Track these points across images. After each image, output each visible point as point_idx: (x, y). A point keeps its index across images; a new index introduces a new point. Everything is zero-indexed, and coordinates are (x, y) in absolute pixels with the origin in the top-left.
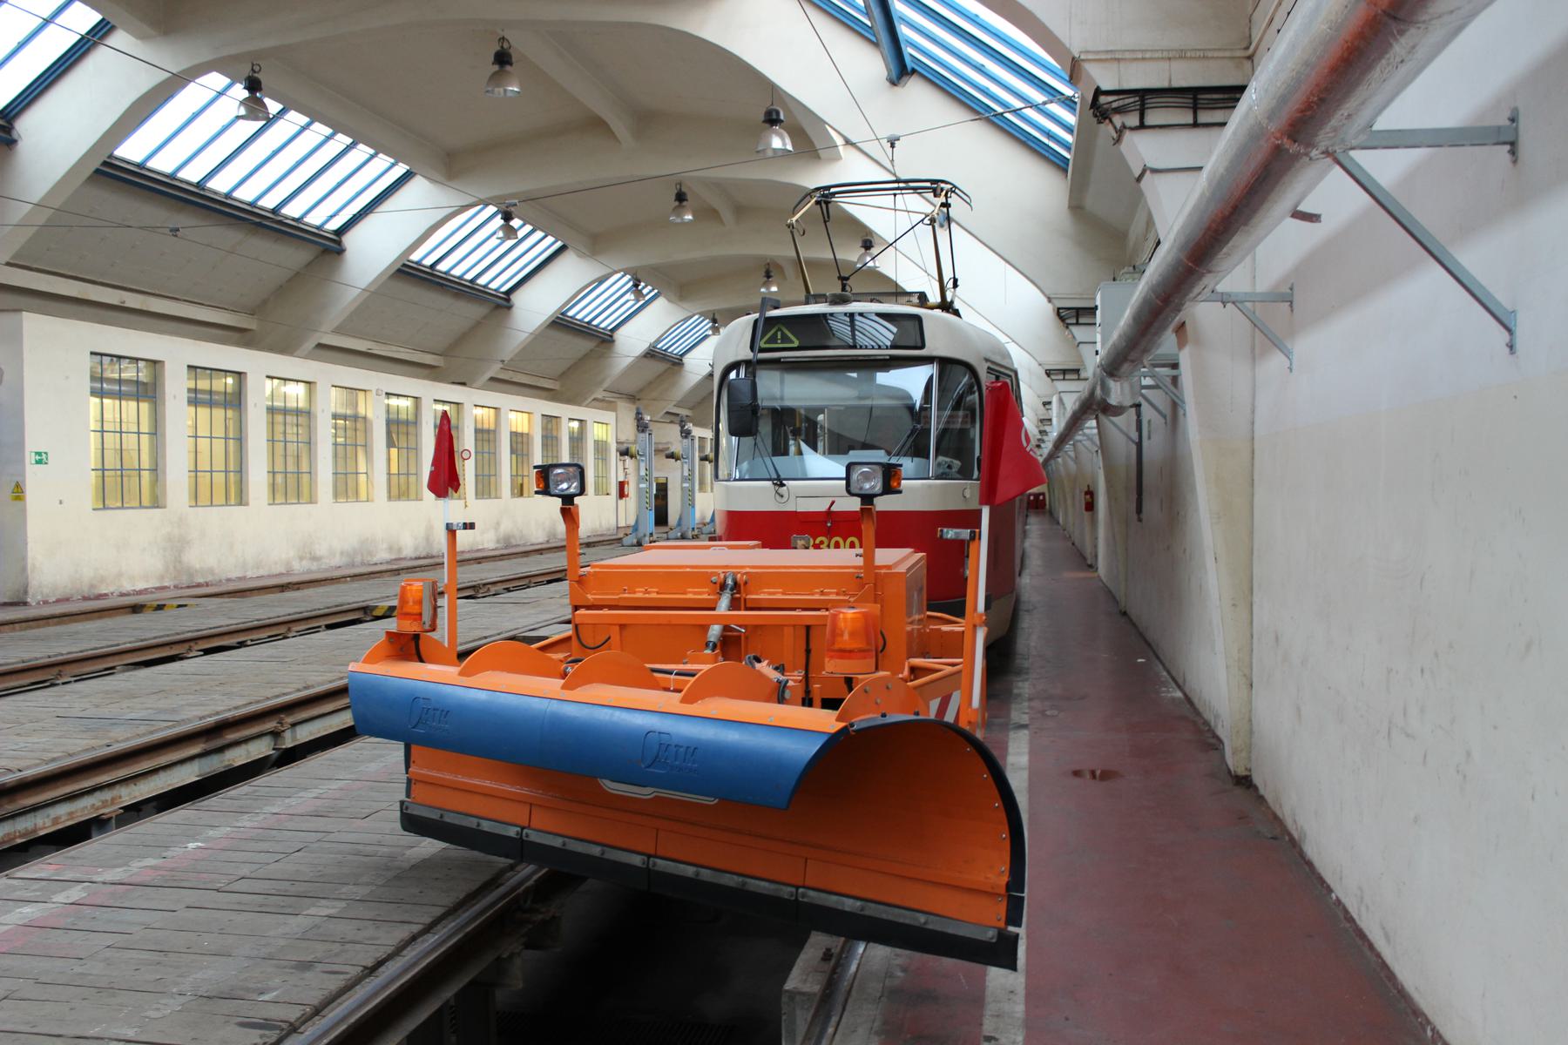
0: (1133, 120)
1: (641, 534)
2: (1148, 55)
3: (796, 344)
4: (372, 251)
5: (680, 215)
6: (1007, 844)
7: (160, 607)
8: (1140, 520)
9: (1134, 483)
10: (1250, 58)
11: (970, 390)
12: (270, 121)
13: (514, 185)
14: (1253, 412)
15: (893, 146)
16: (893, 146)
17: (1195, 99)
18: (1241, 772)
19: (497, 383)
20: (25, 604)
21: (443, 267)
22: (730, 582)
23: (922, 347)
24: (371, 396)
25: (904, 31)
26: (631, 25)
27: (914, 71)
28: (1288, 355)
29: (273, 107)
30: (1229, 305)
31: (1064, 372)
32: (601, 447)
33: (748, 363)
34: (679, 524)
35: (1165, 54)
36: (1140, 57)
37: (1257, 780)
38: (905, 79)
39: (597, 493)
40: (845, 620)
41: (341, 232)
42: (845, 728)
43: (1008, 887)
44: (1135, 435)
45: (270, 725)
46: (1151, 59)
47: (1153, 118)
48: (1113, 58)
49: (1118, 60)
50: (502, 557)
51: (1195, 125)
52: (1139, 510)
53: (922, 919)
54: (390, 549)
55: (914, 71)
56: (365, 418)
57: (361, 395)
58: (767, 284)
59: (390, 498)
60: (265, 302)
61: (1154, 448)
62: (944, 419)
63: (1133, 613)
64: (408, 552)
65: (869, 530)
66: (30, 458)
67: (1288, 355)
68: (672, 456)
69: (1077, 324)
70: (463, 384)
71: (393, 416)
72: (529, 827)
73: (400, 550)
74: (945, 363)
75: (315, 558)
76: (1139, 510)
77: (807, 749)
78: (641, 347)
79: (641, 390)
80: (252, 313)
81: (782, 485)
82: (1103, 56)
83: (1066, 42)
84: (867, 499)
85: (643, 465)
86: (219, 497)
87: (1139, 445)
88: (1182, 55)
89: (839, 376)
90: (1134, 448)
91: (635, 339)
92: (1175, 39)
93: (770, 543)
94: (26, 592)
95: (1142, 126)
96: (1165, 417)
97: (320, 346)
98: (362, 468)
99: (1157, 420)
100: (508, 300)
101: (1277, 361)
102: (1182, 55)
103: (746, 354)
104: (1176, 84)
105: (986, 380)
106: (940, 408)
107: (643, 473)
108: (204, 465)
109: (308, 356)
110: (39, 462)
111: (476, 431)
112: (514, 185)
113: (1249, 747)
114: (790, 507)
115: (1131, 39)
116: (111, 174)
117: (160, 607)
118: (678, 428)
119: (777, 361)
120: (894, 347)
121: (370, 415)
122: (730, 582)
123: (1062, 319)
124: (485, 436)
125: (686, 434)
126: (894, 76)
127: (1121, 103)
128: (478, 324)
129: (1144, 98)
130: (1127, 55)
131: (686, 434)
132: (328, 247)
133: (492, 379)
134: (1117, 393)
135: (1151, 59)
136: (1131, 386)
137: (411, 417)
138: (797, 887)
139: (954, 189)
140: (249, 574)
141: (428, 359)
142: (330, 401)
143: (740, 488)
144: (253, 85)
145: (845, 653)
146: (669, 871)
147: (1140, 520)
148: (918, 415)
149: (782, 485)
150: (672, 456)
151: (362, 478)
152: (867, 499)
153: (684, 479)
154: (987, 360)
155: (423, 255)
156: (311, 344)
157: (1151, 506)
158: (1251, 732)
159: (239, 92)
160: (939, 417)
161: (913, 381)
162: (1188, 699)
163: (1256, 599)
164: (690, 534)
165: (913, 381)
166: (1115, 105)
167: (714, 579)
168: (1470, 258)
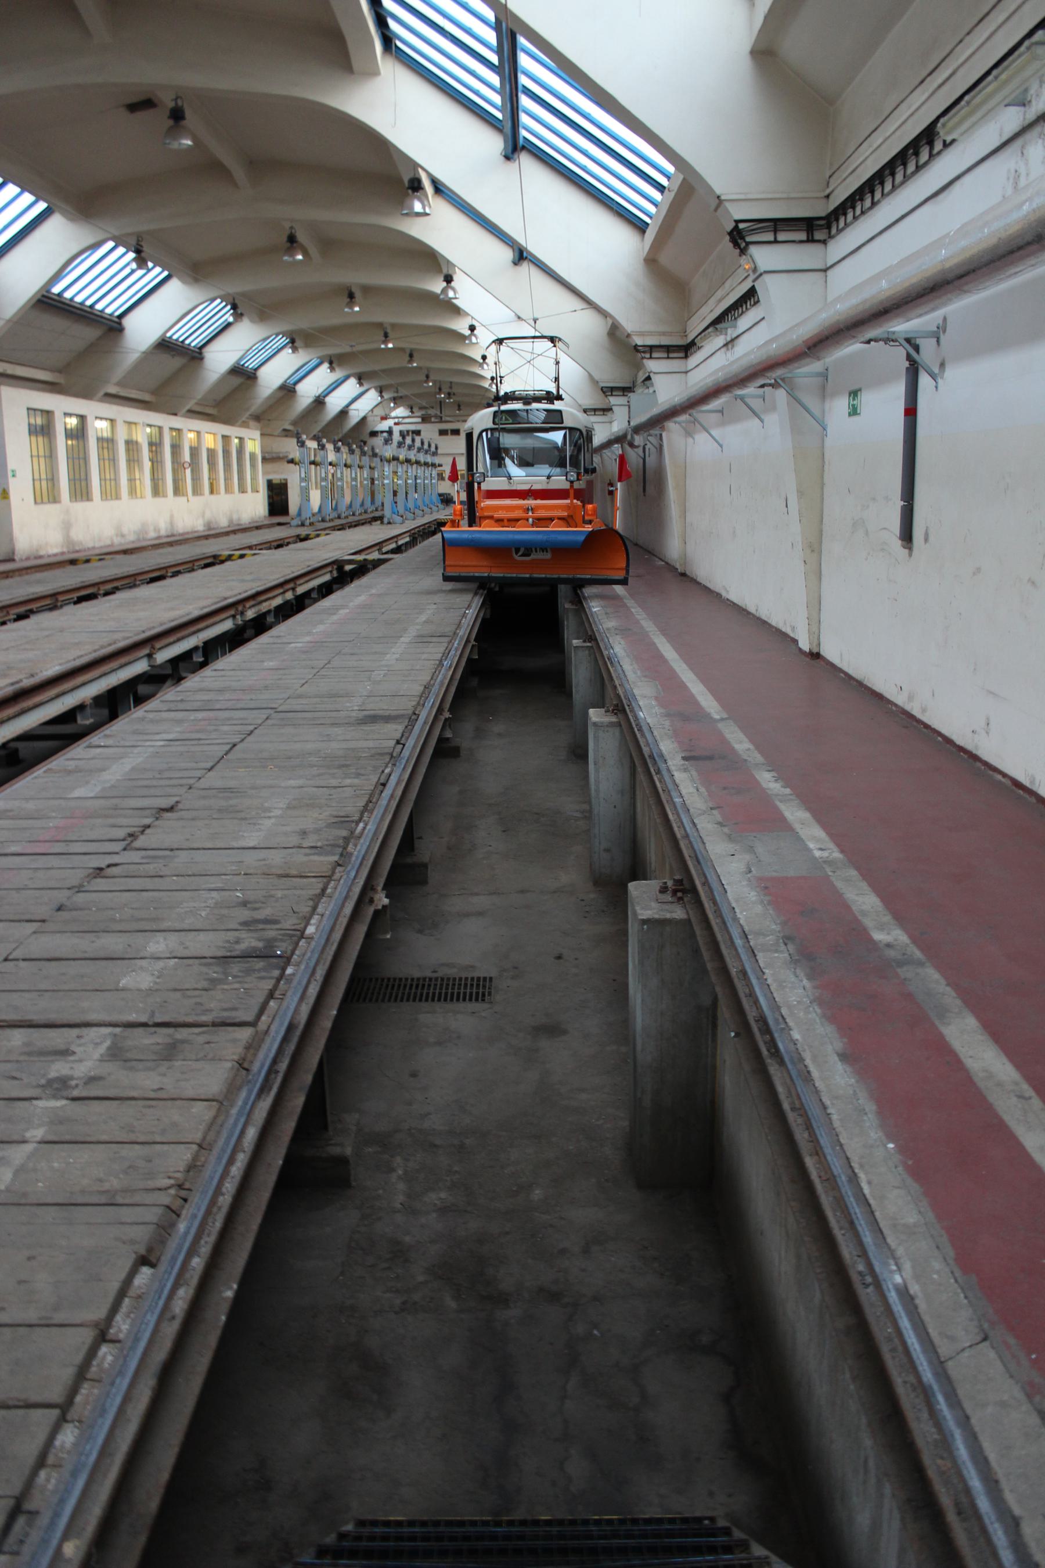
0: (648, 356)
1: (303, 517)
4: (144, 329)
7: (88, 561)
12: (149, 270)
13: (237, 287)
19: (193, 413)
20: (13, 560)
21: (187, 342)
24: (139, 428)
25: (392, 24)
29: (150, 265)
31: (595, 410)
32: (253, 456)
33: (492, 430)
34: (299, 514)
36: (650, 333)
39: (105, 496)
41: (121, 316)
45: (291, 585)
47: (654, 355)
48: (642, 334)
50: (206, 537)
51: (668, 358)
54: (155, 530)
56: (137, 442)
57: (133, 426)
58: (385, 342)
59: (36, 502)
60: (68, 365)
61: (651, 461)
63: (640, 542)
64: (163, 533)
66: (10, 474)
68: (292, 461)
70: (175, 414)
71: (100, 435)
73: (159, 531)
74: (571, 429)
75: (123, 536)
77: (582, 538)
78: (277, 382)
79: (264, 412)
80: (60, 372)
84: (572, 482)
85: (303, 470)
86: (45, 499)
88: (664, 334)
89: (529, 435)
91: (221, 358)
92: (661, 329)
93: (520, 498)
94: (13, 553)
95: (651, 358)
97: (107, 395)
98: (137, 477)
99: (653, 449)
100: (201, 353)
101: (690, 440)
102: (664, 334)
103: (491, 425)
104: (663, 343)
107: (303, 475)
108: (37, 476)
109: (101, 400)
110: (14, 476)
111: (98, 439)
112: (237, 287)
113: (685, 563)
114: (514, 488)
115: (647, 328)
116: (48, 303)
117: (88, 561)
118: (295, 440)
121: (140, 440)
123: (604, 392)
124: (107, 443)
125: (302, 444)
126: (517, 258)
128: (181, 370)
129: (652, 348)
131: (302, 444)
132: (113, 328)
133: (189, 411)
134: (638, 440)
137: (110, 435)
140: (97, 545)
141: (147, 397)
142: (142, 435)
144: (138, 251)
148: (561, 450)
150: (292, 461)
151: (138, 482)
152: (572, 482)
153: (302, 480)
155: (177, 334)
156: (102, 393)
157: (650, 489)
159: (132, 255)
161: (557, 437)
162: (667, 563)
164: (328, 518)
165: (557, 437)
168: (713, 432)
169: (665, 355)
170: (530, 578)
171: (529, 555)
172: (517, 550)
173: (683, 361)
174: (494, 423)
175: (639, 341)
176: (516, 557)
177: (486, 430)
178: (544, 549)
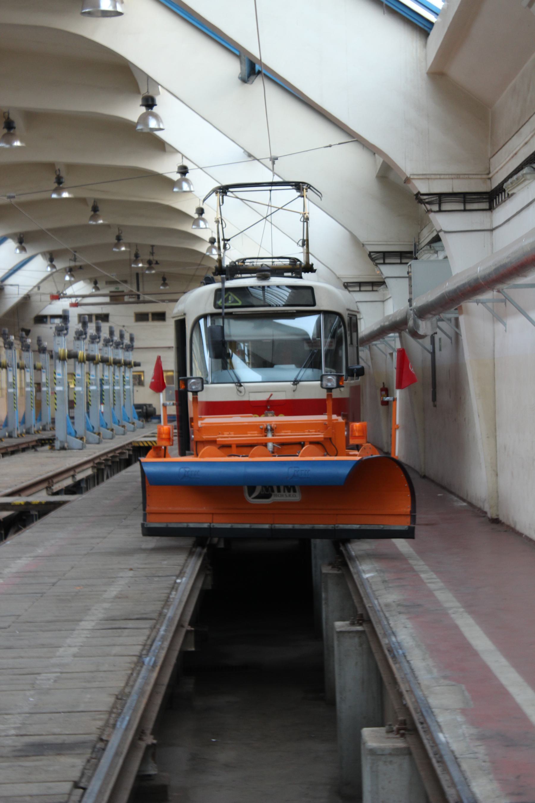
0: (435, 208)
2: (442, 177)
3: (240, 303)
5: (9, 142)
6: (410, 498)
8: (435, 406)
9: (430, 380)
10: (490, 179)
11: (340, 326)
14: (494, 345)
15: (274, 163)
16: (274, 163)
17: (464, 198)
18: (494, 517)
22: (269, 428)
23: (314, 305)
26: (36, 27)
27: (259, 72)
28: (505, 325)
30: (480, 304)
31: (360, 284)
33: (212, 315)
35: (450, 176)
36: (438, 176)
37: (501, 518)
38: (252, 77)
40: (356, 426)
42: (361, 459)
43: (411, 512)
44: (430, 347)
46: (443, 179)
47: (445, 207)
48: (426, 177)
49: (428, 179)
51: (465, 210)
52: (434, 399)
53: (382, 526)
55: (259, 72)
58: (58, 190)
61: (444, 356)
62: (327, 344)
65: (330, 406)
67: (505, 325)
69: (384, 263)
72: (213, 523)
74: (327, 313)
76: (434, 399)
81: (241, 386)
82: (421, 177)
83: (403, 169)
87: (433, 353)
88: (458, 176)
89: (266, 322)
90: (429, 356)
92: (454, 169)
95: (440, 211)
96: (451, 338)
102: (458, 176)
103: (211, 309)
104: (456, 190)
105: (346, 319)
106: (326, 337)
114: (245, 399)
119: (231, 314)
120: (284, 306)
122: (269, 428)
123: (373, 260)
127: (430, 200)
129: (441, 198)
130: (433, 177)
134: (424, 327)
135: (443, 179)
136: (432, 324)
138: (334, 525)
139: (309, 186)
143: (216, 389)
145: (356, 437)
146: (281, 528)
147: (435, 406)
148: (314, 343)
149: (241, 386)
152: (329, 390)
154: (348, 310)
157: (444, 397)
158: (498, 497)
160: (325, 342)
161: (308, 325)
162: (470, 504)
163: (498, 434)
165: (308, 325)
166: (427, 201)
167: (261, 427)
169: (399, 261)
170: (271, 530)
171: (268, 497)
172: (251, 490)
173: (488, 213)
174: (216, 306)
175: (423, 188)
176: (251, 500)
177: (205, 316)
178: (290, 488)
